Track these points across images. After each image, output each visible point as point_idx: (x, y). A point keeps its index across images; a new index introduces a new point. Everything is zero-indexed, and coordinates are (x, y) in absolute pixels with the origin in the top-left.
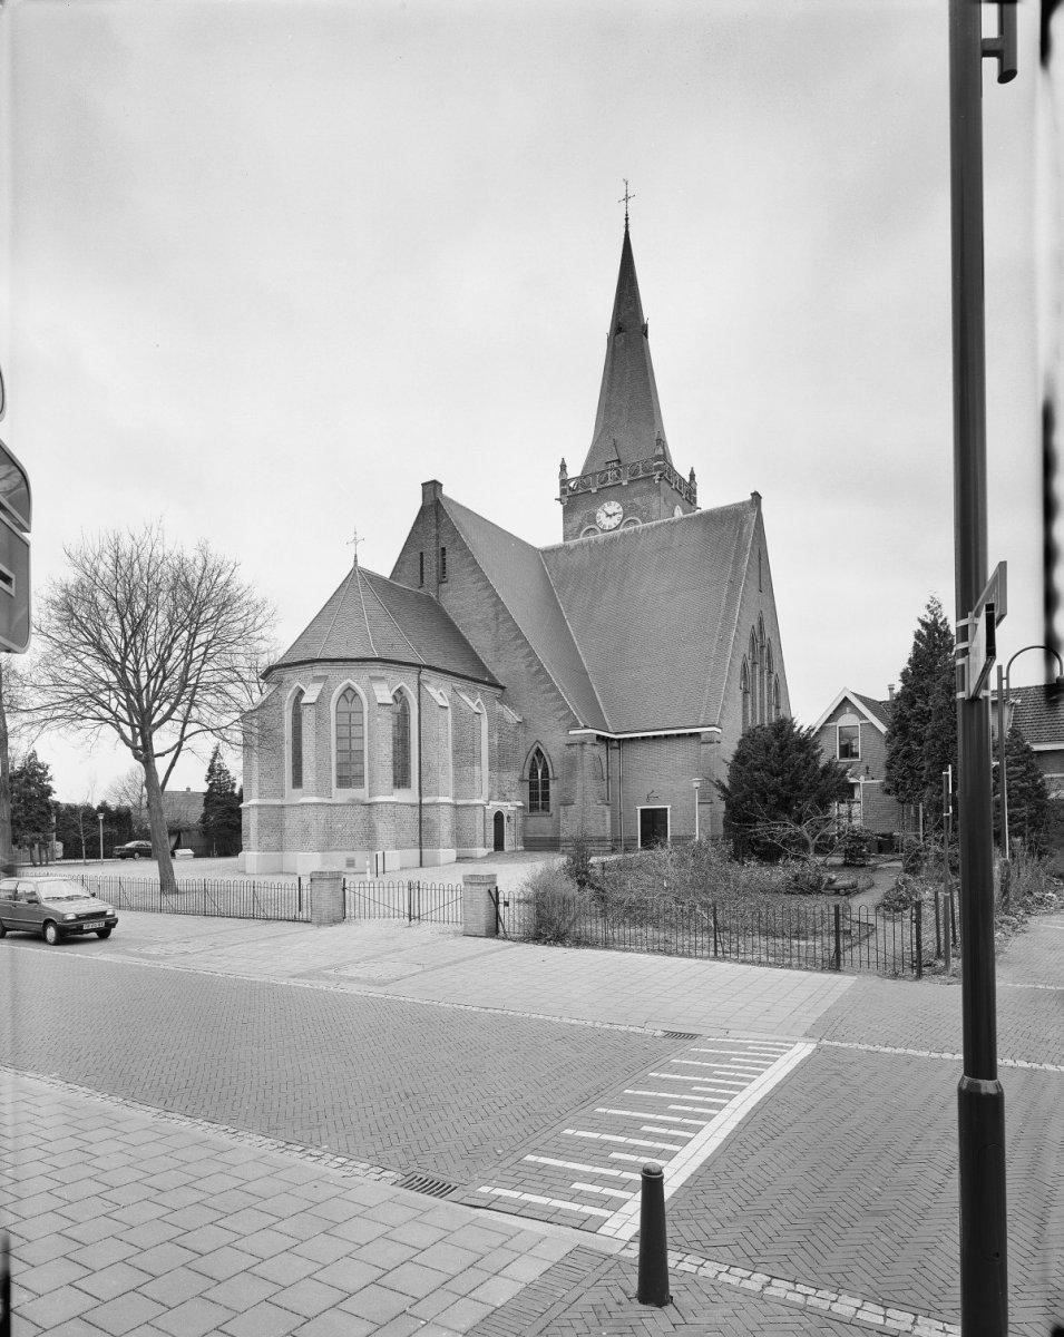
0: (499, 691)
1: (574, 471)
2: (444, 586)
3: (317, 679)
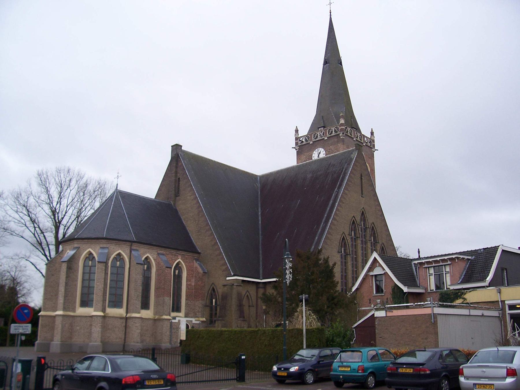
0: (196, 256)
1: (304, 132)
2: (178, 198)
3: (75, 248)
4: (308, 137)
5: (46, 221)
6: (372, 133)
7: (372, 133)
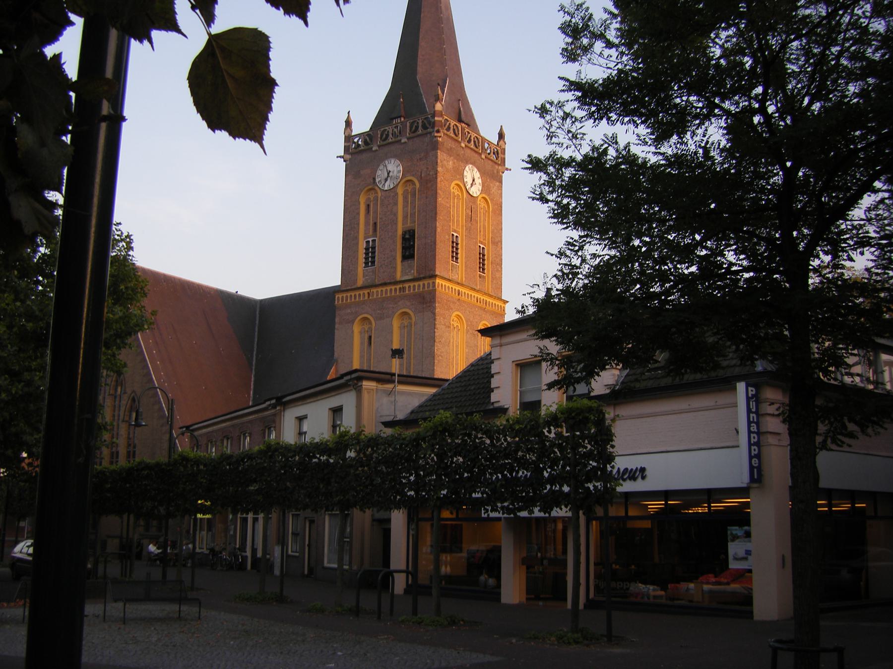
1: (363, 125)
4: (368, 137)
5: (633, 139)
6: (501, 136)
7: (501, 136)
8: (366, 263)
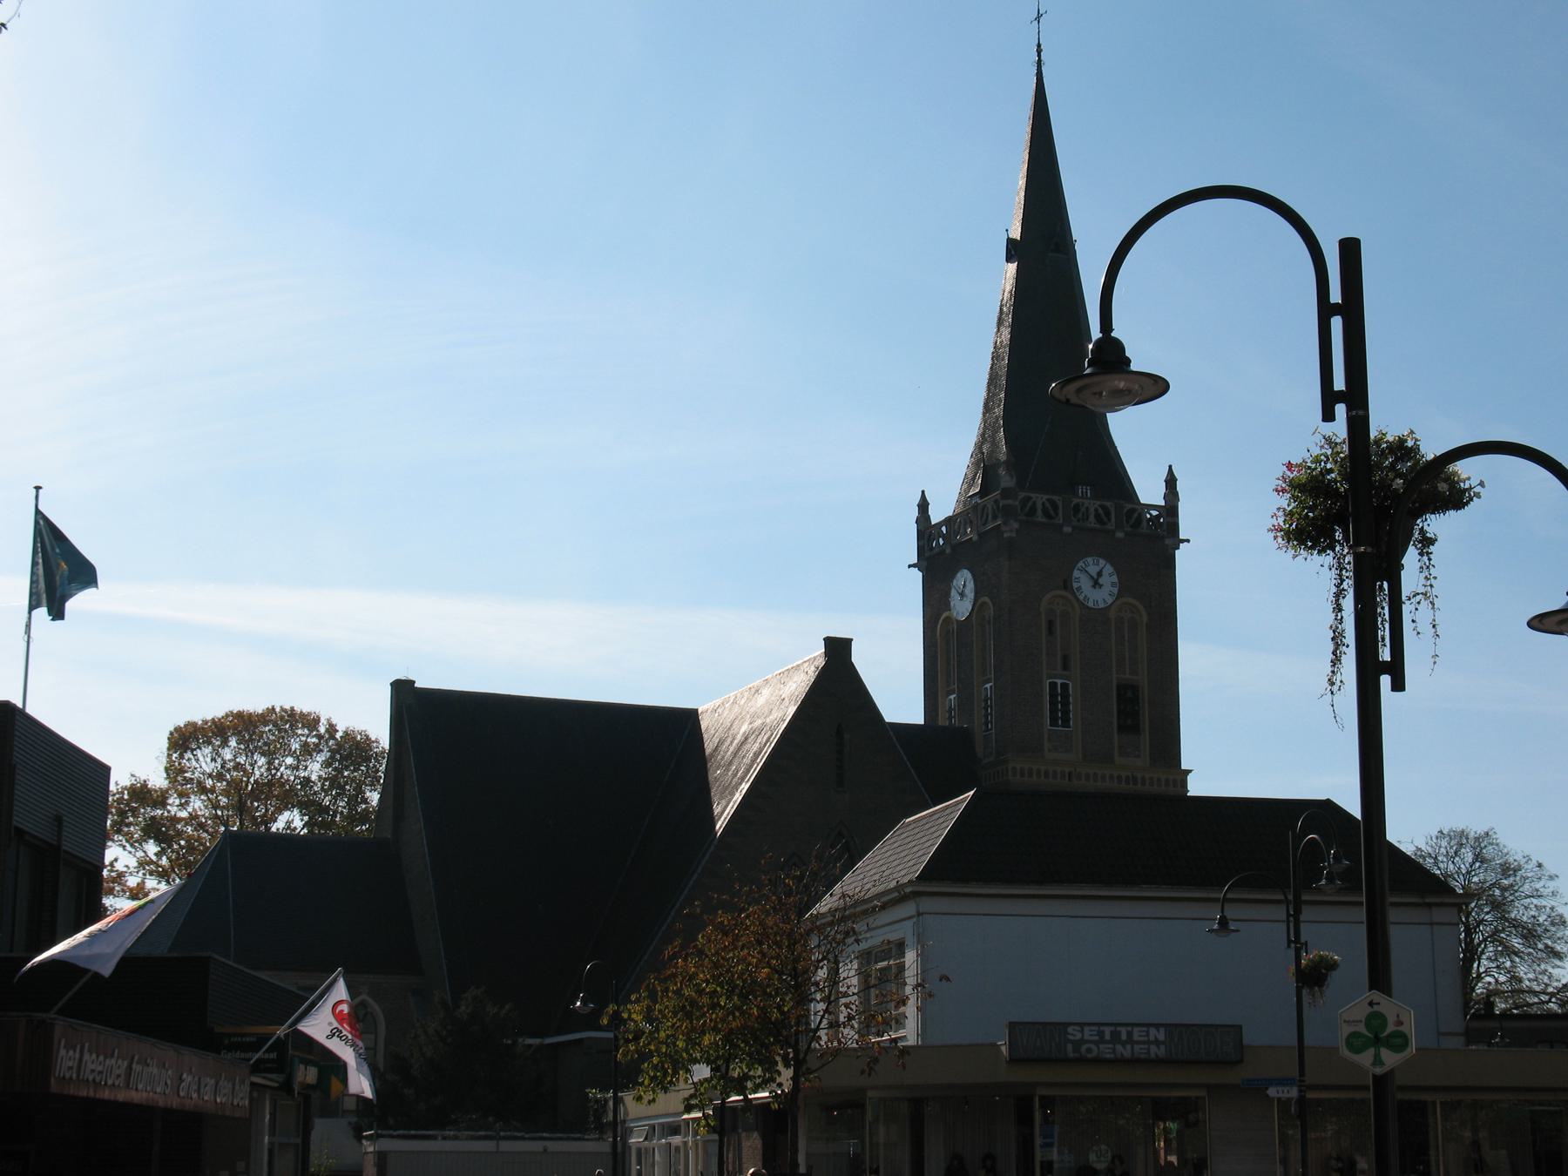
8: (1054, 722)
